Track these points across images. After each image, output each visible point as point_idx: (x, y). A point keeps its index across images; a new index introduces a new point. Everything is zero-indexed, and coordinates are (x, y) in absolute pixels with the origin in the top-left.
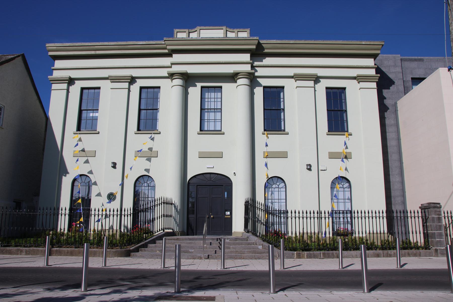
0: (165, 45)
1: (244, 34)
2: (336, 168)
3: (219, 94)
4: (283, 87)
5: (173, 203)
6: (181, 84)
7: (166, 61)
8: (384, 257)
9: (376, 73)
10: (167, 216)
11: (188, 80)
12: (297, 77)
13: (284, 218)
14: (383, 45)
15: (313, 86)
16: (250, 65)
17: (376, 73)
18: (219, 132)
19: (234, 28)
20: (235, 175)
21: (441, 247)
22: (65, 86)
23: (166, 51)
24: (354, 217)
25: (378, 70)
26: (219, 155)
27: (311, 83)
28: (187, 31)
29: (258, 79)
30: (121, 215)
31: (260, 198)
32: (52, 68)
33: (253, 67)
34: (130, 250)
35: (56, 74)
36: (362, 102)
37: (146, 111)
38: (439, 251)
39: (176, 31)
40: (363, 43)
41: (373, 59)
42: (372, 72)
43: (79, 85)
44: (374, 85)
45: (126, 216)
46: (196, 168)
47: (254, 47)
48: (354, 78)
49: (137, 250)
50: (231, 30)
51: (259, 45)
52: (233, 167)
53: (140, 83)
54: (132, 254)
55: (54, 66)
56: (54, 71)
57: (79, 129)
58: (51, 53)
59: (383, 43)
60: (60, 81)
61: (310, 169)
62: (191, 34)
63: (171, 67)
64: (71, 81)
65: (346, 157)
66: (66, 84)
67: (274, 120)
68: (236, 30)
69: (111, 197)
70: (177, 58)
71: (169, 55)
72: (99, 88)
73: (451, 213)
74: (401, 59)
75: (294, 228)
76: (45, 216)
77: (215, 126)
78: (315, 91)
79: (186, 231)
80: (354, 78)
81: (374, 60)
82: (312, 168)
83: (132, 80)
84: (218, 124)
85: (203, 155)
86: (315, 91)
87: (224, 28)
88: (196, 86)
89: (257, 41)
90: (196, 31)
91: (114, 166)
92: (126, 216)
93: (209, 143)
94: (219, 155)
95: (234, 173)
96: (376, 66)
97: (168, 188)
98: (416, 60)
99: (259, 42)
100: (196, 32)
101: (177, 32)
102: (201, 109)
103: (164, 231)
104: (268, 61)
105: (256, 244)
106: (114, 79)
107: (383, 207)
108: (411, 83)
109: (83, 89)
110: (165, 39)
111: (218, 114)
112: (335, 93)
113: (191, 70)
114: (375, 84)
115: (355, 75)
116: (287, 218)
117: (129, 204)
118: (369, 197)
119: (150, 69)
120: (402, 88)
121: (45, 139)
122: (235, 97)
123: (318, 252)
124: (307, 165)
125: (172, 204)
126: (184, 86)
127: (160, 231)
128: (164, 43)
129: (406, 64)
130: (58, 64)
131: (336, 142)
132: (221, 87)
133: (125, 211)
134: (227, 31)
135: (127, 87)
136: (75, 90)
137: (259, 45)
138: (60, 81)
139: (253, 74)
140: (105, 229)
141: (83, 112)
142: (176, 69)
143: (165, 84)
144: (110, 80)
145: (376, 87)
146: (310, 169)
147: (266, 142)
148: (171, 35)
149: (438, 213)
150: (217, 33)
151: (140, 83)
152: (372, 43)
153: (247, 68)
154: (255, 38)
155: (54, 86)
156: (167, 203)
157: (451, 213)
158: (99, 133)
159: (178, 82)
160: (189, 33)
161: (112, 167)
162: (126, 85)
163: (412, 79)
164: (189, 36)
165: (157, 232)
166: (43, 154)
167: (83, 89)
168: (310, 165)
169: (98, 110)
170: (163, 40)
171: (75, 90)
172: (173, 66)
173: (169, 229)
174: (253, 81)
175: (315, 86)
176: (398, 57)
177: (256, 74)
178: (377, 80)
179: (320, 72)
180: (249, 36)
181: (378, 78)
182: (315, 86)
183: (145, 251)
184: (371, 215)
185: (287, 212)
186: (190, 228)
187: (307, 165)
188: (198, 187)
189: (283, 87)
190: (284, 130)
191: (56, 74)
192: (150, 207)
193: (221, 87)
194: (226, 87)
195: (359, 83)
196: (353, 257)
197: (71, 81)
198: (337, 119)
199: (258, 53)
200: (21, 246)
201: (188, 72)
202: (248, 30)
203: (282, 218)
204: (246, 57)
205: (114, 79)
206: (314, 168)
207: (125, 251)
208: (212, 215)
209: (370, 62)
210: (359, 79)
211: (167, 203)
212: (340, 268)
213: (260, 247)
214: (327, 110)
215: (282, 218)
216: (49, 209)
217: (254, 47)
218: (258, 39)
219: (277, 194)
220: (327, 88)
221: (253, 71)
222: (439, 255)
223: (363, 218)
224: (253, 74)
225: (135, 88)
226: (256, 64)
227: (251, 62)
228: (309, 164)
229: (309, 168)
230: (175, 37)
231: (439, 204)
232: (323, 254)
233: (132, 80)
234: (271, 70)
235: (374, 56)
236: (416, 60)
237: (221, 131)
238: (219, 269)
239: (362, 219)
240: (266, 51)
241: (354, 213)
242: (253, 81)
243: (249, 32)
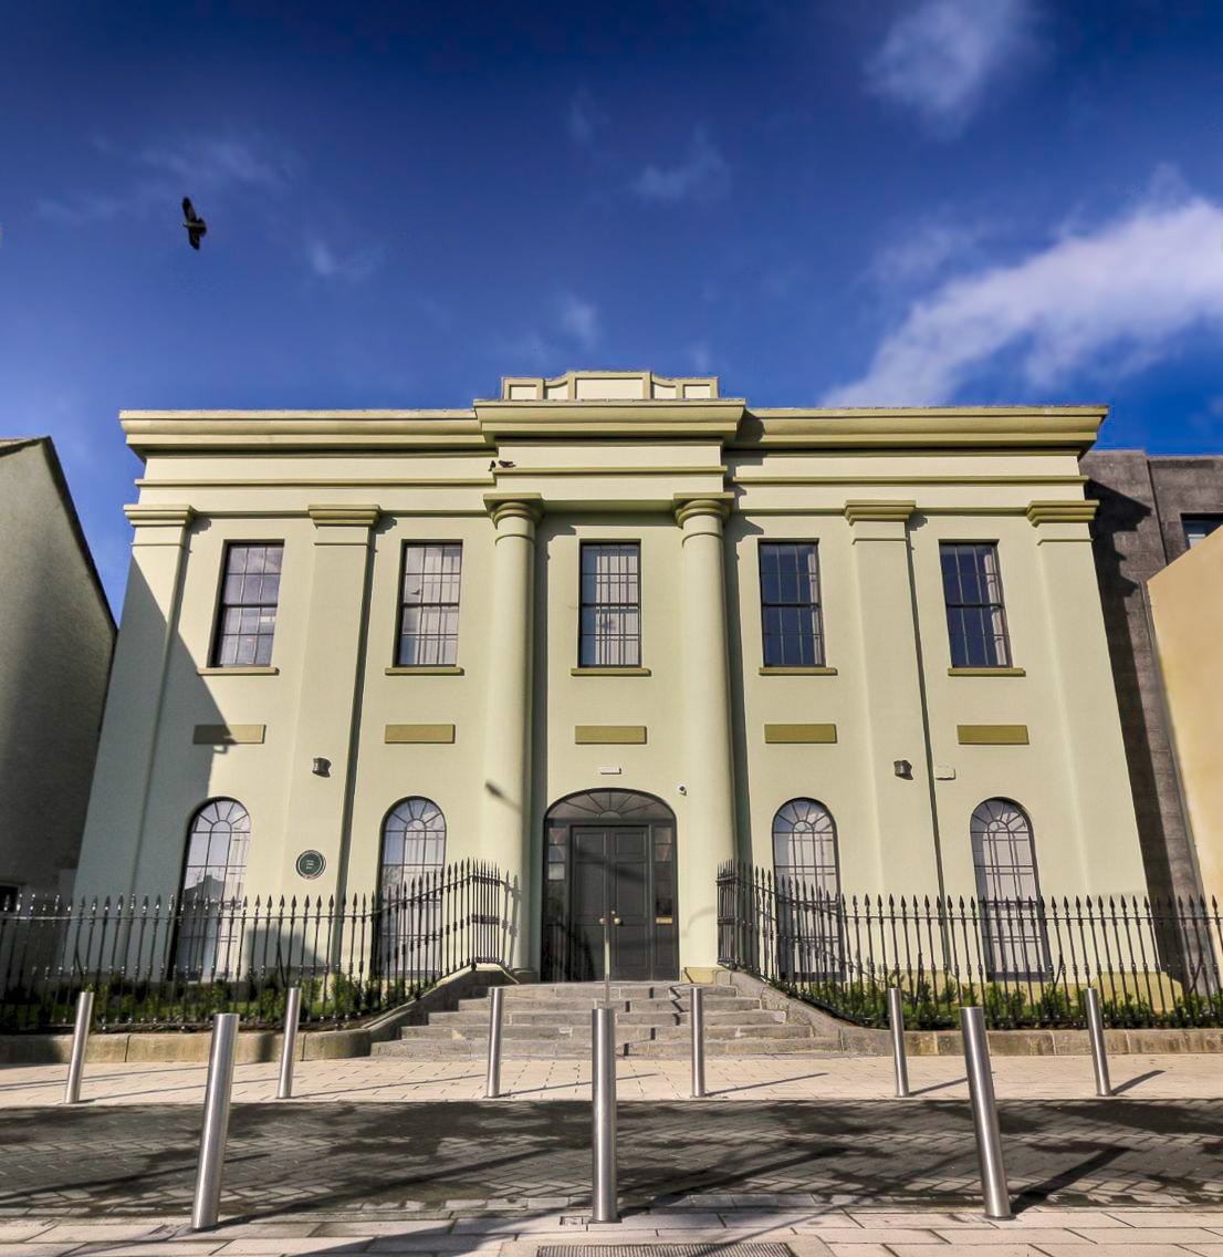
0: (477, 422)
1: (704, 391)
2: (981, 773)
3: (633, 559)
4: (814, 543)
5: (503, 879)
6: (522, 531)
9: (1088, 497)
10: (483, 920)
11: (544, 518)
12: (855, 513)
13: (1033, 924)
14: (1103, 417)
15: (903, 536)
16: (719, 480)
17: (1087, 498)
18: (636, 670)
19: (672, 376)
20: (685, 794)
23: (481, 439)
25: (1092, 489)
26: (638, 737)
27: (898, 529)
28: (539, 382)
29: (747, 518)
30: (340, 918)
31: (762, 858)
32: (137, 482)
33: (729, 484)
34: (368, 1034)
35: (149, 500)
36: (1048, 583)
39: (507, 382)
40: (1047, 411)
41: (1075, 458)
42: (1076, 494)
43: (218, 532)
44: (1083, 530)
45: (359, 920)
46: (570, 773)
47: (733, 427)
48: (1023, 512)
49: (393, 1033)
50: (666, 382)
51: (749, 424)
52: (682, 773)
54: (375, 1046)
55: (142, 477)
56: (144, 492)
58: (132, 439)
59: (1104, 411)
60: (159, 519)
61: (907, 775)
62: (550, 390)
63: (495, 484)
64: (195, 521)
67: (793, 634)
68: (678, 382)
69: (310, 864)
72: (280, 543)
74: (1148, 463)
75: (879, 951)
76: (86, 924)
77: (622, 652)
78: (909, 549)
79: (538, 967)
80: (1023, 512)
81: (1079, 459)
82: (912, 772)
83: (381, 520)
84: (632, 647)
85: (588, 737)
86: (909, 549)
87: (646, 375)
89: (742, 409)
90: (566, 383)
91: (323, 768)
92: (359, 920)
93: (605, 701)
94: (638, 737)
95: (682, 789)
96: (1086, 477)
97: (490, 838)
98: (1190, 465)
99: (745, 412)
100: (566, 387)
101: (511, 386)
102: (582, 605)
103: (474, 966)
104: (773, 466)
105: (765, 1007)
106: (324, 518)
107: (1136, 883)
108: (1180, 529)
109: (229, 545)
110: (476, 402)
111: (632, 618)
112: (967, 561)
113: (554, 492)
114: (1085, 526)
115: (1025, 504)
116: (1043, 922)
117: (362, 884)
118: (1087, 852)
120: (1155, 543)
121: (106, 695)
122: (680, 564)
124: (897, 764)
125: (497, 883)
126: (533, 536)
127: (462, 966)
128: (473, 415)
129: (1163, 476)
130: (156, 468)
131: (983, 699)
132: (637, 543)
133: (355, 903)
134: (652, 383)
135: (366, 541)
136: (207, 545)
137: (749, 424)
138: (159, 519)
139: (731, 503)
140: (289, 968)
142: (509, 488)
143: (476, 533)
144: (315, 518)
145: (1087, 536)
146: (907, 775)
147: (772, 697)
148: (495, 394)
150: (629, 388)
151: (404, 529)
152: (1072, 411)
153: (714, 486)
154: (736, 401)
155: (141, 535)
156: (485, 879)
158: (277, 672)
159: (515, 525)
160: (546, 388)
161: (314, 772)
163: (1184, 517)
164: (545, 396)
165: (455, 970)
166: (98, 739)
167: (229, 545)
168: (907, 766)
169: (275, 606)
170: (471, 406)
171: (207, 545)
172: (500, 481)
173: (489, 961)
174: (730, 520)
175: (908, 534)
176: (1139, 454)
178: (1092, 517)
179: (924, 498)
180: (716, 396)
181: (1093, 510)
182: (908, 534)
183: (417, 1034)
184: (1100, 911)
185: (1041, 904)
186: (562, 952)
187: (897, 764)
188: (575, 830)
189: (814, 543)
190: (823, 665)
191: (149, 500)
192: (428, 895)
193: (637, 543)
194: (651, 536)
195: (1036, 525)
196: (1150, 1047)
197: (195, 521)
198: (975, 633)
199: (743, 444)
202: (713, 382)
203: (1027, 923)
204: (710, 455)
205: (324, 518)
206: (919, 770)
207: (352, 1036)
208: (616, 916)
209: (1068, 465)
210: (1040, 514)
211: (485, 880)
212: (1099, 1094)
213: (780, 1016)
214: (947, 606)
215: (1027, 923)
216: (102, 902)
217: (733, 427)
218: (743, 403)
219: (805, 852)
220: (943, 543)
221: (731, 495)
223: (1109, 923)
224: (731, 503)
225: (388, 542)
226: (743, 472)
227: (725, 468)
228: (901, 760)
230: (506, 397)
233: (381, 520)
234: (778, 494)
235: (1080, 448)
236: (1190, 465)
237: (639, 666)
238: (686, 1096)
239: (1104, 924)
240: (765, 439)
241: (950, 906)
242: (730, 520)
243: (715, 387)
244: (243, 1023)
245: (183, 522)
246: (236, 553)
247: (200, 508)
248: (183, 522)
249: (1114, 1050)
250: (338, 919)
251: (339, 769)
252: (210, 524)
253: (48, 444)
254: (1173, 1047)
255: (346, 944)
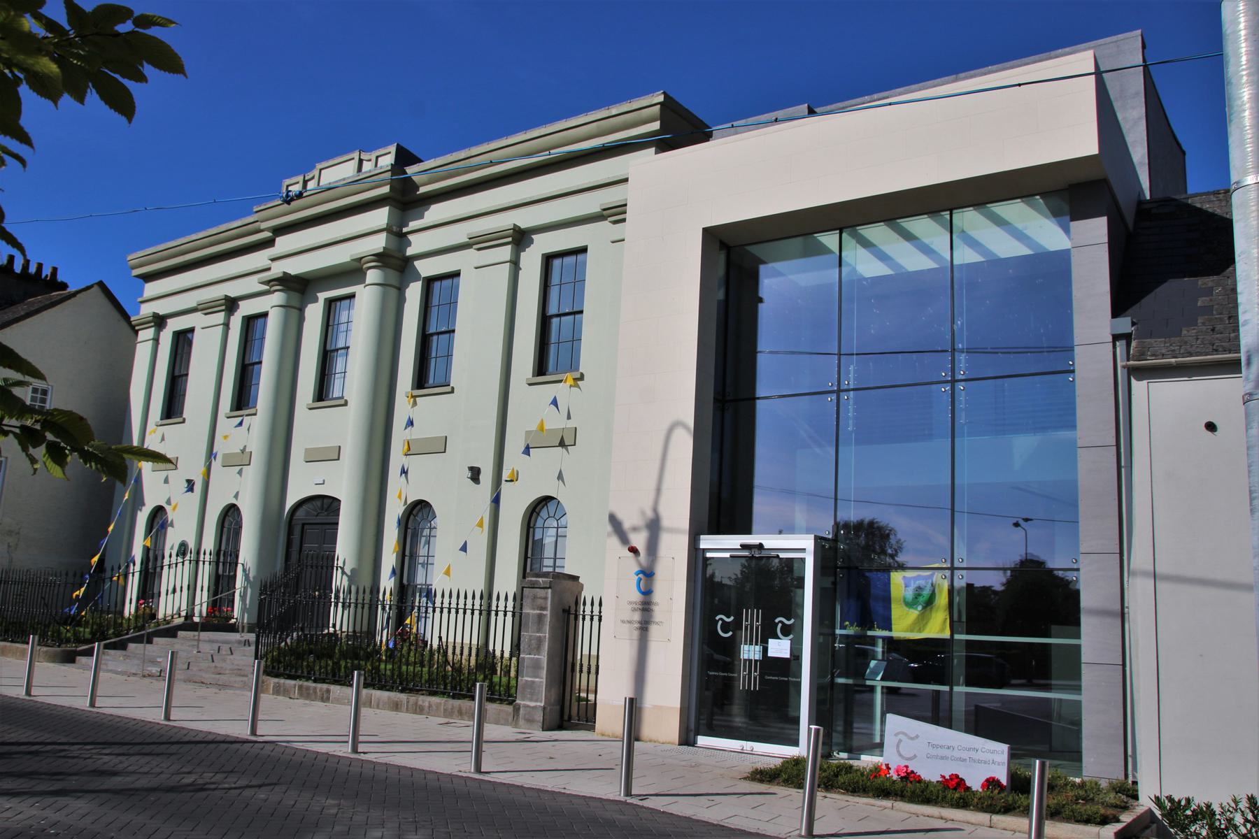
7: (259, 259)
8: (407, 711)
11: (299, 288)
21: (531, 700)
22: (220, 317)
24: (497, 612)
37: (571, 317)
38: (522, 711)
53: (544, 244)
57: (541, 368)
60: (145, 324)
65: (562, 444)
66: (223, 314)
70: (285, 243)
71: (269, 243)
73: (600, 604)
83: (521, 238)
88: (316, 300)
91: (475, 474)
104: (436, 212)
109: (548, 259)
119: (242, 276)
123: (292, 682)
136: (531, 261)
138: (145, 324)
141: (555, 321)
142: (278, 269)
147: (533, 404)
149: (540, 602)
157: (600, 604)
158: (452, 392)
162: (220, 317)
169: (581, 312)
177: (410, 252)
179: (525, 219)
187: (471, 469)
199: (406, 200)
200: (308, 679)
201: (293, 273)
204: (380, 217)
206: (198, 487)
222: (521, 722)
229: (475, 474)
231: (576, 578)
232: (300, 687)
233: (521, 238)
240: (422, 190)
241: (584, 604)
244: (1052, 801)
245: (510, 239)
246: (557, 263)
247: (524, 224)
248: (510, 239)
249: (365, 705)
250: (487, 612)
251: (198, 487)
252: (532, 241)
253: (101, 284)
254: (396, 707)
255: (198, 601)
